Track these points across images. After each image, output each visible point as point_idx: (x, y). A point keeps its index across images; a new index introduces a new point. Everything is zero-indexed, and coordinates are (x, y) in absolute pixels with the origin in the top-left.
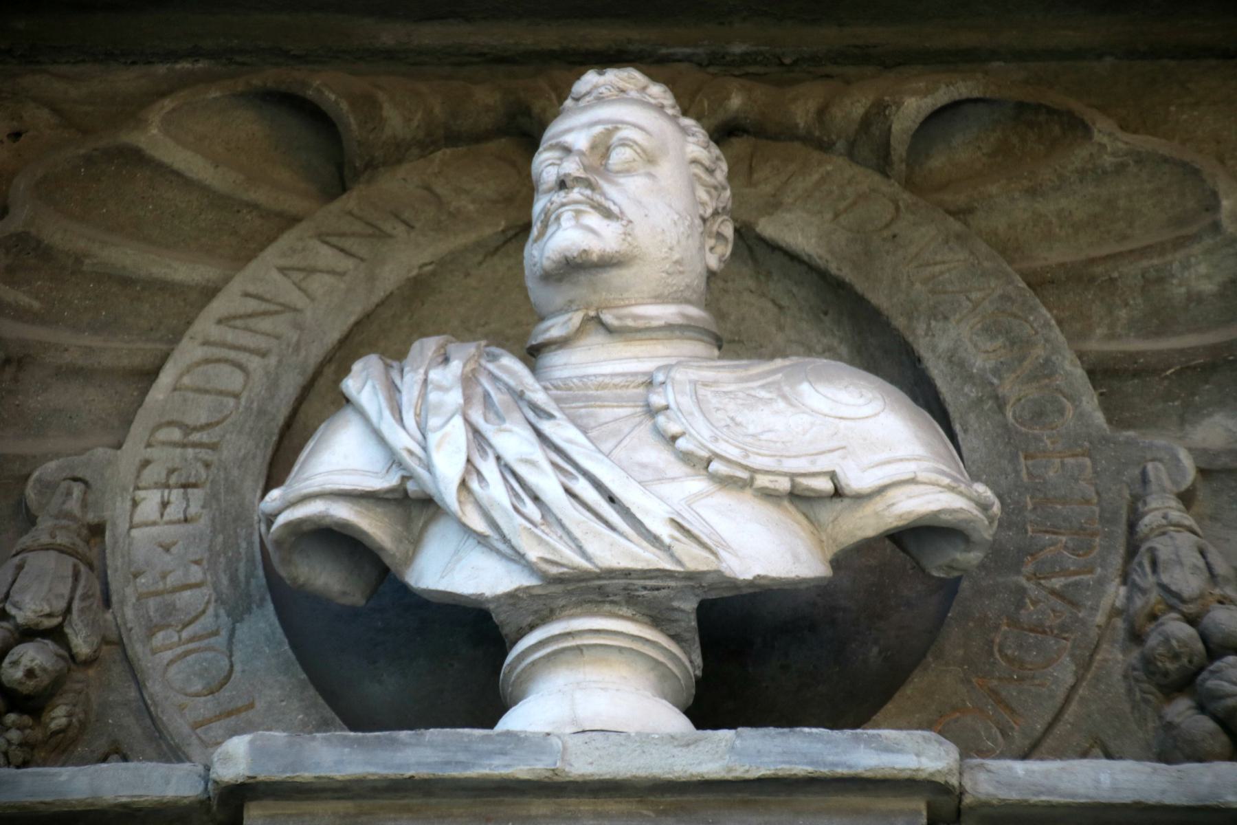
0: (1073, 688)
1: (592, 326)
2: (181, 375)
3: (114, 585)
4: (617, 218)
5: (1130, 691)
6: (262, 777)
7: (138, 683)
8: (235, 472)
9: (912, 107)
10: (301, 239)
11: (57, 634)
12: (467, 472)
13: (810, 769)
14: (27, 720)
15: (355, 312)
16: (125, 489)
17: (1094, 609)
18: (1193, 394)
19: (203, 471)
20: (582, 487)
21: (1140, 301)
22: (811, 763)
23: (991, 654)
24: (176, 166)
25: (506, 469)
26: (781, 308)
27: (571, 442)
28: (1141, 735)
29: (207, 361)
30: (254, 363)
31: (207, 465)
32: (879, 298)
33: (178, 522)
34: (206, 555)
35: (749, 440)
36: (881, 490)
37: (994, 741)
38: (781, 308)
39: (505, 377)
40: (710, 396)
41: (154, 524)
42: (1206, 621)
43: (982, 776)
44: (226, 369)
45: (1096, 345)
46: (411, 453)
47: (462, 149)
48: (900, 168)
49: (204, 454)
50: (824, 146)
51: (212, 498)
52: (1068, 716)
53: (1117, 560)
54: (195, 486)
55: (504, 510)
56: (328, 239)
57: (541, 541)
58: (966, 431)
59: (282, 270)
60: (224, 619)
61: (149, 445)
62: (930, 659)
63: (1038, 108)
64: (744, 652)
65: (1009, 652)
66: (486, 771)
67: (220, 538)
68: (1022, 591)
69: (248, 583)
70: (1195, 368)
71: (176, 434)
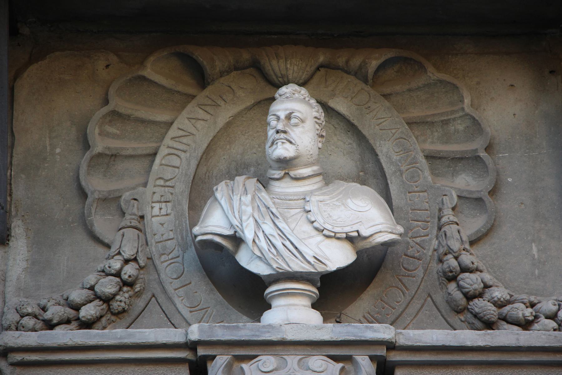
0: (423, 278)
1: (287, 175)
2: (162, 160)
3: (149, 239)
4: (294, 144)
5: (438, 278)
6: (202, 339)
7: (158, 273)
8: (180, 197)
9: (374, 64)
10: (193, 107)
11: (135, 260)
12: (255, 236)
13: (354, 338)
14: (129, 288)
15: (212, 135)
16: (149, 203)
17: (429, 250)
18: (456, 166)
19: (170, 196)
20: (288, 243)
21: (441, 130)
22: (354, 336)
23: (400, 266)
24: (155, 81)
25: (265, 235)
26: (335, 128)
27: (284, 228)
28: (441, 293)
29: (169, 154)
30: (183, 155)
31: (172, 194)
32: (365, 132)
33: (165, 215)
34: (174, 228)
35: (334, 222)
36: (371, 235)
38: (335, 128)
39: (264, 201)
40: (322, 205)
41: (158, 216)
42: (460, 259)
43: (401, 336)
44: (174, 157)
45: (430, 147)
46: (238, 226)
47: (239, 72)
48: (370, 82)
49: (171, 190)
50: (348, 73)
51: (174, 207)
53: (435, 232)
54: (168, 202)
55: (266, 251)
56: (201, 107)
58: (391, 183)
59: (188, 118)
60: (181, 252)
61: (155, 186)
63: (411, 59)
64: (333, 291)
65: (405, 266)
66: (264, 338)
67: (177, 221)
68: (408, 243)
69: (186, 239)
70: (456, 158)
71: (161, 182)
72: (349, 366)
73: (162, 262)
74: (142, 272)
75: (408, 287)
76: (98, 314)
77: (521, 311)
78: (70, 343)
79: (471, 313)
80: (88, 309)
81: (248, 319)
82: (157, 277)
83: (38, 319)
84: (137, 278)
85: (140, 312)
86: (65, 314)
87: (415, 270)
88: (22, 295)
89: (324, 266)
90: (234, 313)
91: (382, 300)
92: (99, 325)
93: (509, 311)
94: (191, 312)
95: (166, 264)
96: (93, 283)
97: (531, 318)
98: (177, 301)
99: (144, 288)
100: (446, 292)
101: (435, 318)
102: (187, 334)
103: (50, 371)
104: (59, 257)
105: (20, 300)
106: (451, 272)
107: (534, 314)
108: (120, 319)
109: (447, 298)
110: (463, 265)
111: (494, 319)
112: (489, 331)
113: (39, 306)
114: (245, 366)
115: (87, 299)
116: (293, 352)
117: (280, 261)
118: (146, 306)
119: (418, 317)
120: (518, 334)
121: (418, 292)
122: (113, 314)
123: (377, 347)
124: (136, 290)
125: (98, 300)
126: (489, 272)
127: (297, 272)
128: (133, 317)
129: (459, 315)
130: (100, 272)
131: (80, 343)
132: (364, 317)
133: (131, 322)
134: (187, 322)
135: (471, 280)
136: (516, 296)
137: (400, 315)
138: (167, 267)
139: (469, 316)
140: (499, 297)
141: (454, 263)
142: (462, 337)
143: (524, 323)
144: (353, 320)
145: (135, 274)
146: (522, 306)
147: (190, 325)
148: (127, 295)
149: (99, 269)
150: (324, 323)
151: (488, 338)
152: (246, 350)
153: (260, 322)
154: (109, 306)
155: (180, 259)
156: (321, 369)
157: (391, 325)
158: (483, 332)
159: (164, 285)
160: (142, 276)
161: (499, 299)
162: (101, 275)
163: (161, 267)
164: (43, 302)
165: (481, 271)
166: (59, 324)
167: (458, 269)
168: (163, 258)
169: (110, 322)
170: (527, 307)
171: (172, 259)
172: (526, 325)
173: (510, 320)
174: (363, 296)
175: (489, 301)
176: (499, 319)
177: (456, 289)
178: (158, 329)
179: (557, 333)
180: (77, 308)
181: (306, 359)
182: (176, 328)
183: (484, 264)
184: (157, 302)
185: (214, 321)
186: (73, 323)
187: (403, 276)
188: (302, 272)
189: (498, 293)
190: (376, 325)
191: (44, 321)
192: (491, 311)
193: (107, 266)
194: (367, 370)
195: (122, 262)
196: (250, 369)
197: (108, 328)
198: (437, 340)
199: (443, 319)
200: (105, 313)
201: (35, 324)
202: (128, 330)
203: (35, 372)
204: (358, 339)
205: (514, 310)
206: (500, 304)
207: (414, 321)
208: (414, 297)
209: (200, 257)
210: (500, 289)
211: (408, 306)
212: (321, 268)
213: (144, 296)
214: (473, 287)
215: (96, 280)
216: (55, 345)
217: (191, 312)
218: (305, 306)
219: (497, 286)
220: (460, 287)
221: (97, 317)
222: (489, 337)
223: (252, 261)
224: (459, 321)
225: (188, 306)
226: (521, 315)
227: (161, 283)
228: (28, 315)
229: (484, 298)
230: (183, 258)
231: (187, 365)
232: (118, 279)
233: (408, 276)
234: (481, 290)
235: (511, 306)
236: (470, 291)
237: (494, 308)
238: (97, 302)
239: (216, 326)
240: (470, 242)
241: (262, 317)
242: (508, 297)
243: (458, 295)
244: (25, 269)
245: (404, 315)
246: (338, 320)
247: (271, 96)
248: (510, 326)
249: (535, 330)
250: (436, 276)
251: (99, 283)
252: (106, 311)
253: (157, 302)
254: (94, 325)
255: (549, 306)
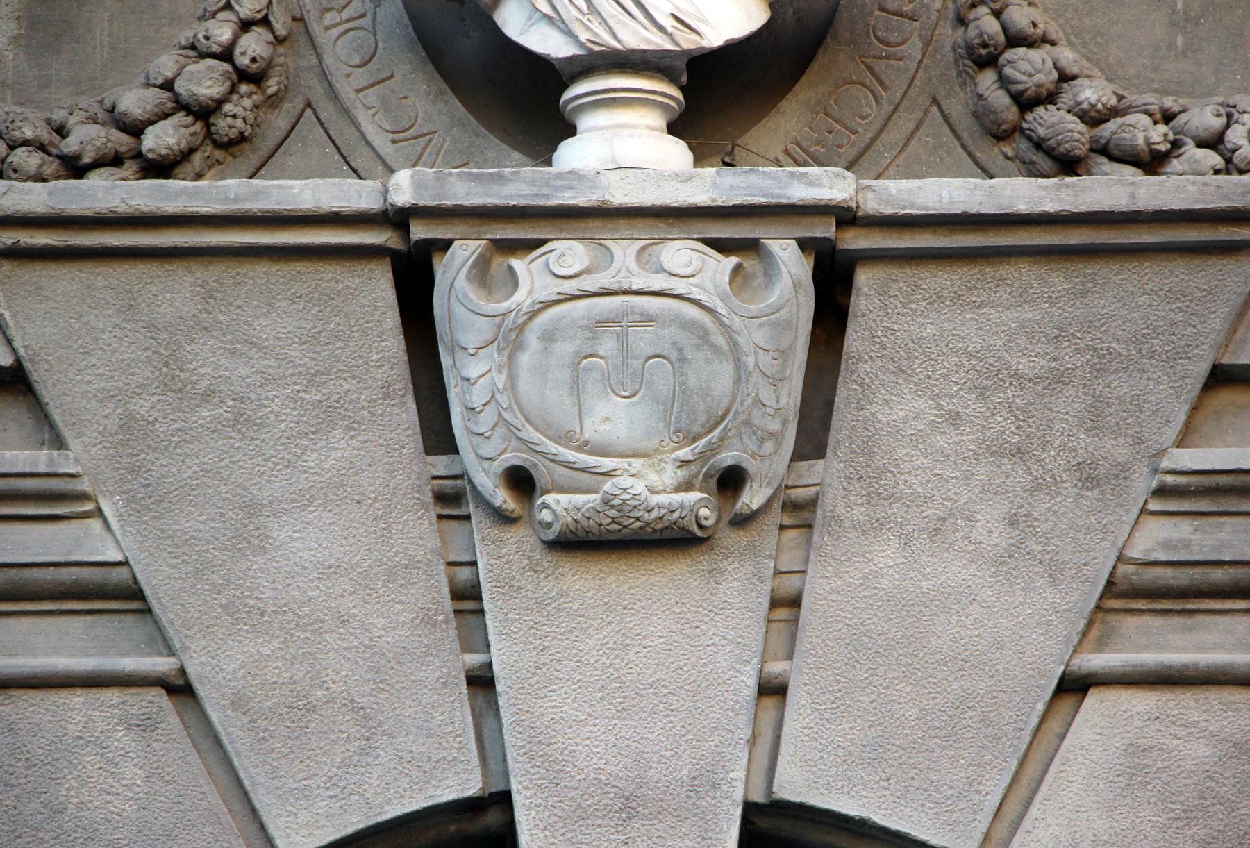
0: (921, 61)
5: (956, 61)
6: (421, 203)
11: (265, 22)
14: (252, 87)
22: (763, 196)
23: (868, 36)
28: (962, 95)
37: (870, 107)
42: (1005, 16)
43: (870, 195)
52: (917, 82)
57: (588, 28)
60: (369, 5)
62: (829, 40)
65: (880, 33)
66: (561, 202)
72: (752, 262)
73: (327, 28)
74: (281, 50)
75: (887, 83)
76: (183, 145)
77: (1144, 132)
78: (122, 209)
79: (1030, 139)
80: (161, 134)
81: (525, 159)
82: (315, 61)
83: (49, 154)
84: (270, 64)
85: (279, 141)
86: (109, 144)
87: (903, 43)
88: (9, 98)
89: (695, 37)
90: (493, 145)
91: (826, 114)
92: (186, 169)
93: (1115, 133)
94: (394, 142)
95: (335, 32)
96: (170, 74)
97: (1163, 147)
98: (362, 117)
99: (286, 87)
100: (972, 92)
101: (948, 153)
102: (385, 192)
103: (80, 271)
104: (91, 11)
105: (6, 109)
106: (985, 45)
107: (1171, 137)
108: (235, 157)
109: (976, 105)
110: (1013, 30)
111: (1081, 150)
112: (1068, 179)
113: (49, 124)
114: (517, 264)
115: (157, 110)
116: (626, 233)
117: (596, 26)
118: (293, 128)
119: (909, 149)
120: (1133, 184)
121: (909, 94)
122: (218, 145)
123: (817, 219)
124: (270, 91)
125: (182, 113)
126: (1070, 44)
127: (634, 51)
128: (264, 152)
129: (1001, 144)
130: (184, 48)
131: (146, 209)
132: (787, 152)
133: (258, 165)
134: (385, 164)
135: (1031, 64)
136: (1132, 98)
137: (868, 147)
138: (338, 38)
139: (1024, 145)
140: (1093, 100)
141: (991, 26)
142: (1008, 193)
143: (1147, 159)
144: (761, 160)
145: (265, 55)
146: (1145, 120)
147: (392, 171)
148: (247, 103)
149: (183, 43)
150: (695, 166)
151: (1066, 194)
152: (517, 229)
153: (551, 165)
154: (208, 126)
155: (366, 22)
156: (689, 271)
157: (847, 169)
158: (1055, 180)
159: (333, 80)
160: (281, 60)
161: (1093, 106)
162: (187, 57)
163: (325, 39)
164: (58, 115)
165: (1053, 43)
166: (97, 164)
167: (1002, 38)
168: (329, 18)
169: (212, 163)
170: (1156, 123)
171: (348, 21)
172: (1152, 162)
173: (1116, 153)
174: (784, 104)
175: (1069, 112)
176: (1092, 150)
177: (996, 86)
178: (321, 181)
179: (1221, 178)
180: (135, 130)
181: (654, 247)
182: (360, 178)
183: (1061, 26)
184: (318, 118)
185: (448, 164)
186: (128, 163)
187: (874, 57)
188: (644, 51)
189: (1091, 92)
190: (814, 170)
191: (62, 158)
192: (1074, 133)
193: (200, 36)
194: (793, 271)
195: (235, 27)
196: (529, 271)
197: (207, 176)
198: (952, 202)
199: (964, 155)
200: (198, 142)
201: (41, 166)
202: (253, 181)
203: (44, 273)
204: (773, 201)
205: (1127, 129)
206: (1093, 118)
207: (900, 161)
208: (899, 104)
209: (412, 17)
210: (1096, 82)
211: (885, 125)
212: (688, 42)
213: (287, 106)
214: (1035, 79)
215: (176, 67)
216: (89, 213)
217: (394, 142)
218: (652, 129)
219: (1088, 77)
220: (1004, 82)
221: (181, 152)
222: (1067, 191)
223: (532, 25)
224: (1002, 157)
225: (388, 128)
226: (1141, 141)
227: (324, 76)
228: (25, 143)
229: (1059, 105)
230: (374, 18)
231: (388, 260)
232: (226, 66)
233: (888, 57)
234: (1052, 87)
235: (1119, 120)
236: (1027, 89)
237: (1081, 127)
238: (180, 118)
239: (451, 174)
240: (799, 606)
241: (556, 154)
242: (1114, 101)
243: (1000, 100)
244: (15, 40)
245: (878, 146)
246: (727, 160)
247: (391, 163)
248: (1116, 166)
249: (1171, 173)
250: (950, 56)
251: (185, 74)
252: (201, 137)
253: (318, 118)
254: (176, 171)
255: (1205, 118)
